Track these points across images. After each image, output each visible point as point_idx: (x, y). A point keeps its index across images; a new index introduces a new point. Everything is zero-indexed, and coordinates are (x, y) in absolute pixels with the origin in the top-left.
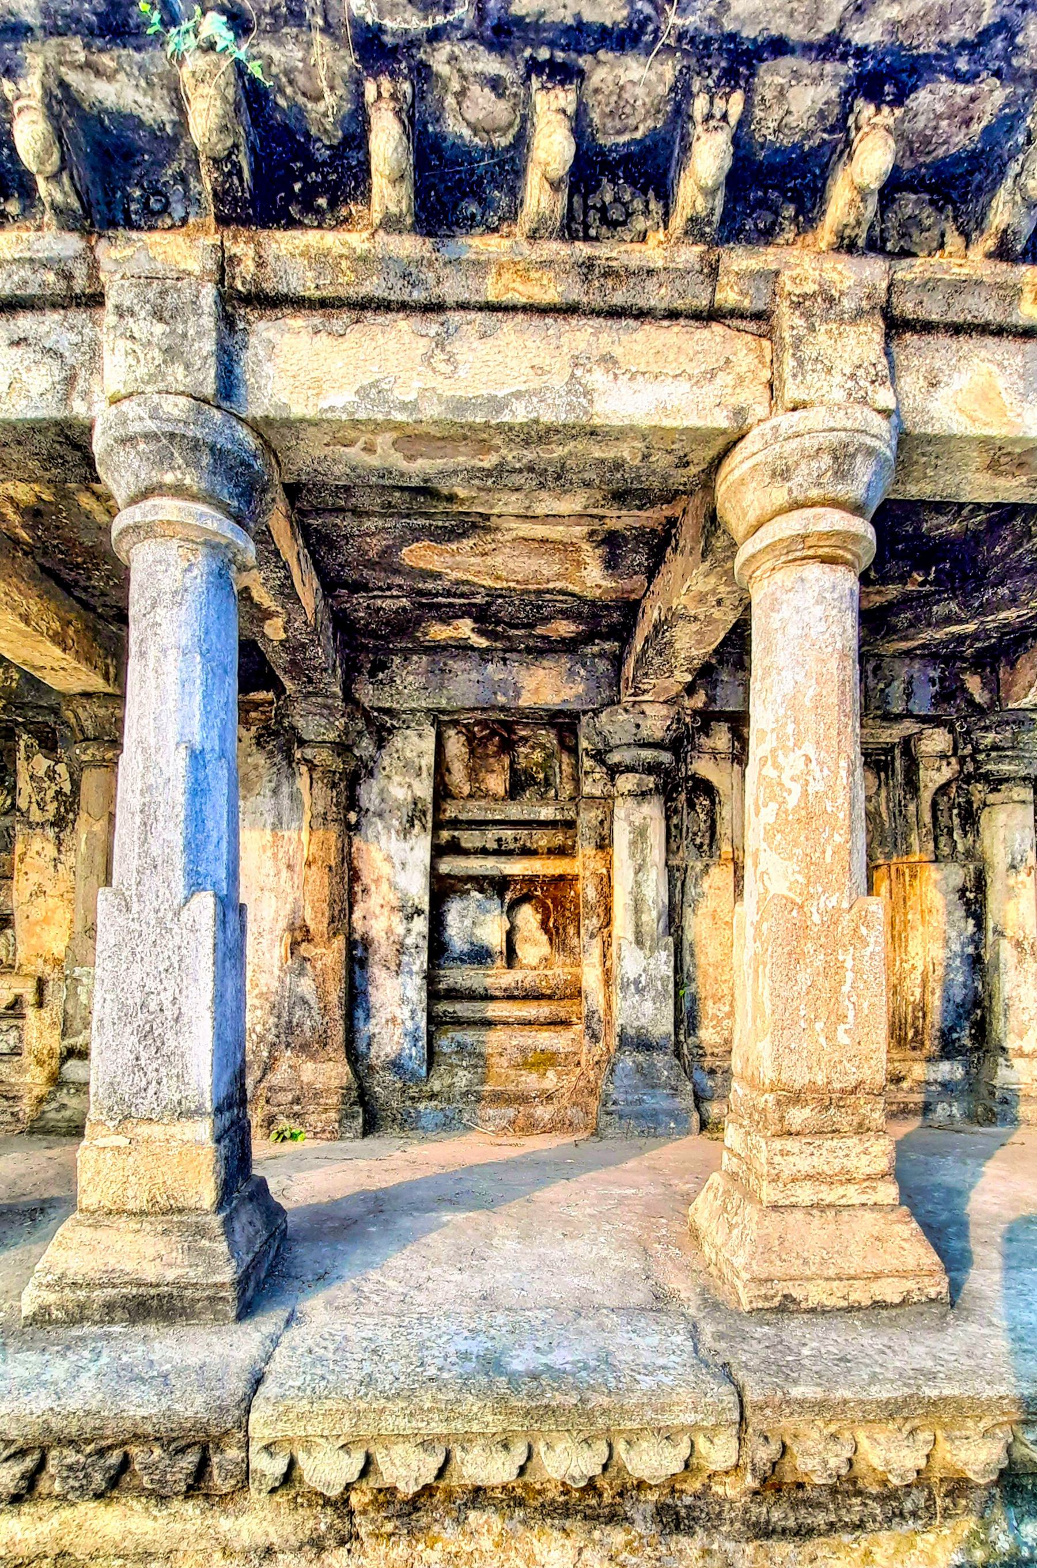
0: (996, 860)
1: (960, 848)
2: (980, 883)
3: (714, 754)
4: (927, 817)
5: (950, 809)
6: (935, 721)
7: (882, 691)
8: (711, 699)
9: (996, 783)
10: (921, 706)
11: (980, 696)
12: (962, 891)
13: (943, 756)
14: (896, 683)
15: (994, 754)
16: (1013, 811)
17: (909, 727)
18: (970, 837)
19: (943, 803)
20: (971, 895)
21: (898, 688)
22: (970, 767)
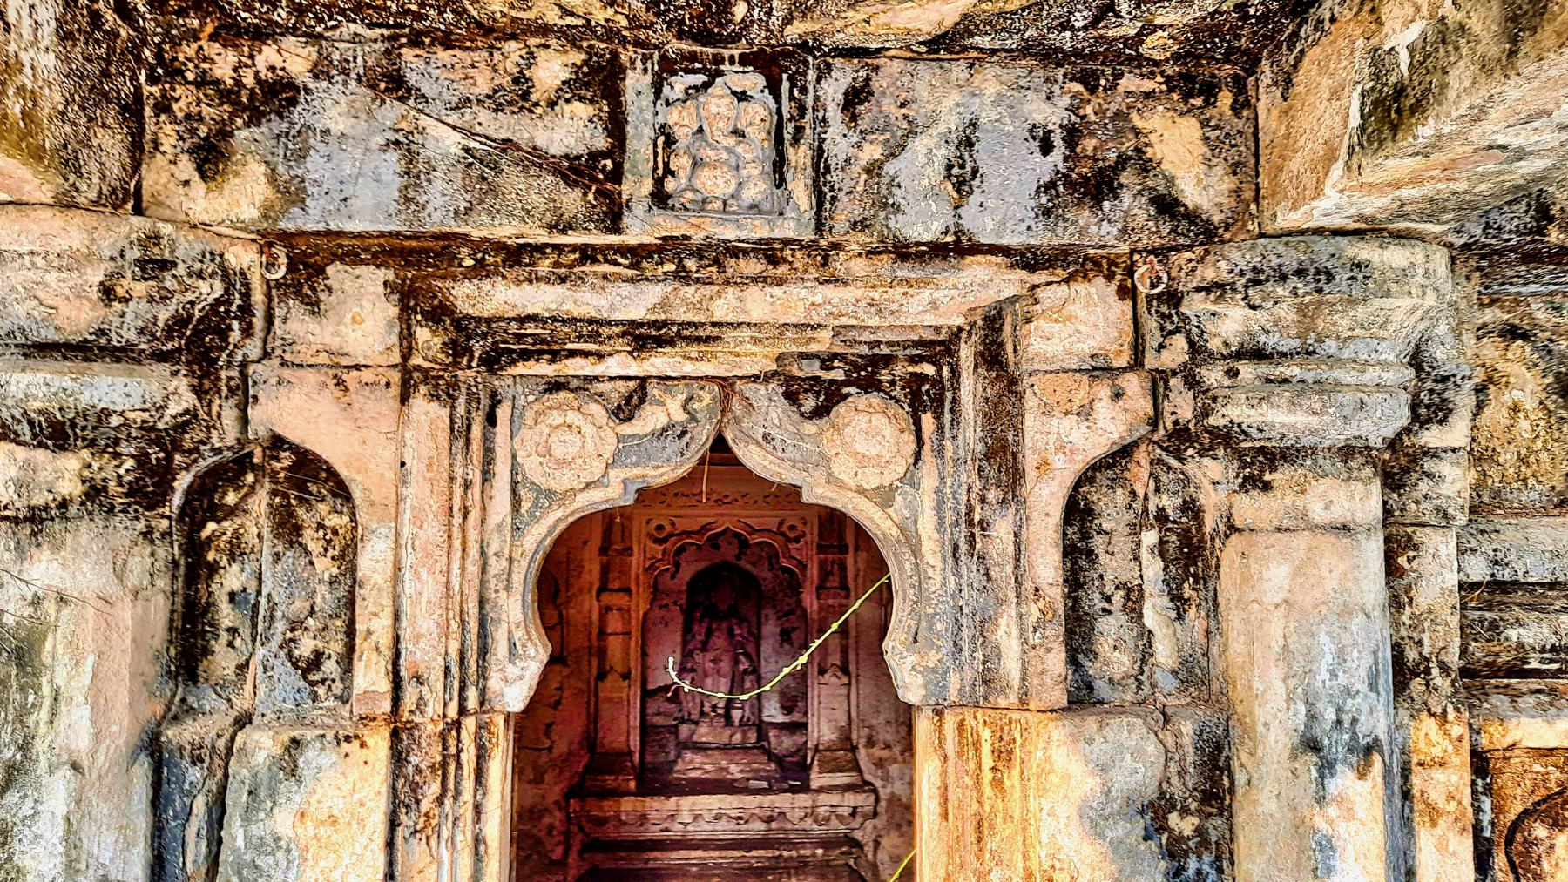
0: (1262, 714)
1: (1164, 653)
2: (1215, 778)
3: (340, 372)
4: (1047, 567)
5: (1134, 529)
6: (1073, 263)
7: (873, 169)
8: (292, 194)
9: (1260, 462)
10: (1006, 208)
11: (1205, 189)
12: (1158, 810)
13: (1099, 370)
14: (919, 145)
15: (1247, 370)
16: (1311, 559)
17: (985, 282)
18: (1195, 619)
19: (1112, 509)
20: (1184, 825)
21: (924, 160)
22: (1182, 406)
